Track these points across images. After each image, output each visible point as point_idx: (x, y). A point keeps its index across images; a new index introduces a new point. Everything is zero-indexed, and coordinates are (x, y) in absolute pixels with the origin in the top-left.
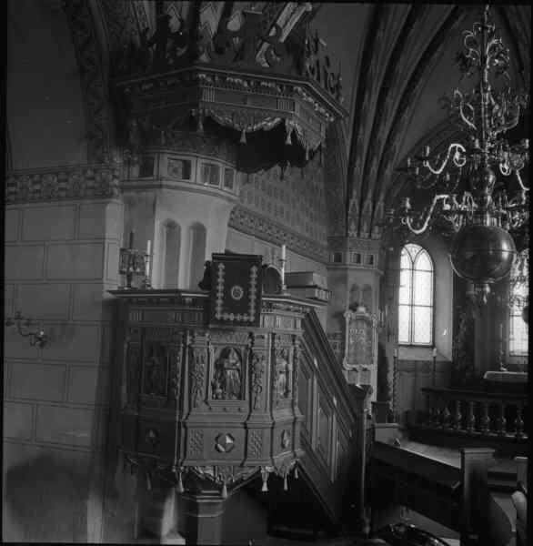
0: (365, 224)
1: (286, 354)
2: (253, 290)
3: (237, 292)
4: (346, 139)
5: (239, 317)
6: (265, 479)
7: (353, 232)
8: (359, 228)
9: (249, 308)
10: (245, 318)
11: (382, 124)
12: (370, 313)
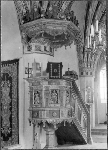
1: (68, 92)
3: (55, 70)
4: (82, 39)
5: (56, 77)
6: (65, 122)
7: (86, 66)
8: (87, 65)
9: (54, 76)
11: (89, 17)
12: (92, 89)
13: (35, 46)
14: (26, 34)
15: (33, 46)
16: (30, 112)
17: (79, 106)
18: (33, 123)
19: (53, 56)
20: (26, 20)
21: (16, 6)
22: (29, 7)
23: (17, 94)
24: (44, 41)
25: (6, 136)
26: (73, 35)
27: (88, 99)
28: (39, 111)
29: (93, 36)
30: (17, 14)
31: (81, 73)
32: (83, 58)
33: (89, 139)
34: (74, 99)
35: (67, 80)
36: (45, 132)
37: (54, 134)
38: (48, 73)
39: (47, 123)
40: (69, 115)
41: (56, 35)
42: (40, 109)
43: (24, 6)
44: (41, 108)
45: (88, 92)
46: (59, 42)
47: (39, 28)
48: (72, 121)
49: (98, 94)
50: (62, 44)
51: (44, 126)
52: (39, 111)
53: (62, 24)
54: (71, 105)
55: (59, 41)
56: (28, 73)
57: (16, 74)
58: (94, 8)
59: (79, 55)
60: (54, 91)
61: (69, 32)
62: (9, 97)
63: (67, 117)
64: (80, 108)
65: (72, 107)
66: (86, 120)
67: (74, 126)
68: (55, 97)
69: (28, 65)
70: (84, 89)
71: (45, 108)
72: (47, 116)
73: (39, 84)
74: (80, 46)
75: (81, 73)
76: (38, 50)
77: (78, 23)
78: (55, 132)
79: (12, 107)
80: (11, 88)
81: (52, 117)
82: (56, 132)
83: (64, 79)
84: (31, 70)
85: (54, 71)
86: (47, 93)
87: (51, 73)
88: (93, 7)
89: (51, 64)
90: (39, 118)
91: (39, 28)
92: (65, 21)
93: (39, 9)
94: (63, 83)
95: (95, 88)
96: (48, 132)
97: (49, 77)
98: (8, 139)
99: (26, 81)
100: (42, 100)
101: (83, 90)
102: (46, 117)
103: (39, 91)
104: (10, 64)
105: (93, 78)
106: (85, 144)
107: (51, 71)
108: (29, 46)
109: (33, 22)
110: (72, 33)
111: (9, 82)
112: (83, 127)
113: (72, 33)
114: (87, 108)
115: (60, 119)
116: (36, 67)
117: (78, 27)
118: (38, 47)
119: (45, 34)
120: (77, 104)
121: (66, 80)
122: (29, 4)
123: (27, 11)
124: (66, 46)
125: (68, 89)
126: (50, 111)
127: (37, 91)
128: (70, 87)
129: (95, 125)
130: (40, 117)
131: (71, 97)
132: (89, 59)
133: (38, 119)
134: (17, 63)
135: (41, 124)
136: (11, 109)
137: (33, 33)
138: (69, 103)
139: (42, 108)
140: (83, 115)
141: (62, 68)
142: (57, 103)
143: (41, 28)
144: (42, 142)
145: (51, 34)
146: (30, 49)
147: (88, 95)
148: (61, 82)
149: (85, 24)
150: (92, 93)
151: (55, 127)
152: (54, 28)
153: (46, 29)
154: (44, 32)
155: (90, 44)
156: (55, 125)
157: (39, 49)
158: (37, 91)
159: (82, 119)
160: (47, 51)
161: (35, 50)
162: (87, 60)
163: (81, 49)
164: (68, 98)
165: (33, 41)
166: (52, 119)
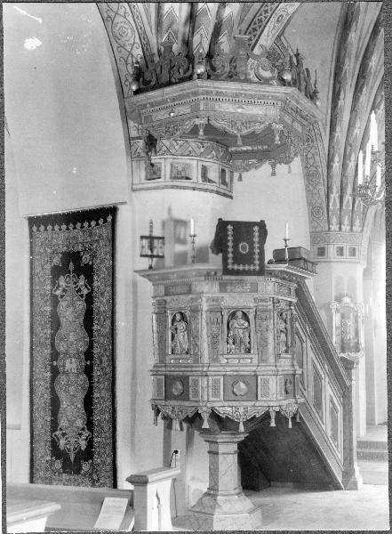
0: (346, 219)
2: (257, 245)
5: (247, 267)
6: (273, 415)
7: (334, 227)
9: (254, 259)
10: (252, 268)
11: (347, 60)
13: (172, 165)
14: (145, 125)
15: (165, 163)
16: (159, 382)
17: (316, 361)
18: (164, 418)
19: (231, 197)
20: (146, 83)
21: (110, 34)
22: (153, 40)
23: (108, 322)
24: (202, 150)
25: (72, 459)
26: (300, 129)
27: (342, 340)
28: (188, 377)
29: (376, 149)
30: (112, 62)
31: (319, 249)
32: (324, 198)
33: (348, 473)
34: (300, 337)
35: (283, 276)
36: (207, 446)
37: (235, 452)
38: (217, 254)
39: (214, 416)
40: (287, 392)
41: (245, 132)
42: (194, 369)
43: (137, 34)
44: (192, 367)
45: (343, 316)
46: (252, 151)
47: (189, 110)
48: (297, 411)
49: (375, 321)
50: (262, 156)
51: (206, 425)
52: (187, 378)
53: (264, 96)
54: (293, 358)
55: (249, 148)
56: (150, 253)
57: (108, 256)
58: (365, 32)
59: (311, 188)
60: (239, 314)
61: (288, 119)
62: (83, 333)
63: (279, 398)
64: (319, 367)
65: (295, 363)
66: (340, 408)
67: (299, 424)
68: (241, 331)
69: (151, 227)
70: (329, 304)
71: (210, 369)
72: (216, 394)
73: (189, 292)
74: (317, 157)
75: (319, 249)
76: (182, 178)
77: (315, 92)
78: (239, 447)
79: (92, 365)
80: (89, 299)
81: (232, 395)
82: (241, 445)
83: (271, 273)
84: (160, 245)
85: (238, 248)
86: (215, 320)
87: (230, 255)
88: (363, 25)
89: (230, 227)
90: (188, 399)
91: (189, 110)
92: (277, 90)
93: (187, 43)
94: (268, 287)
95: (366, 301)
96: (216, 445)
97: (221, 268)
98: (80, 468)
99: (139, 278)
100: (199, 343)
101: (327, 307)
102: (210, 398)
103: (188, 314)
104: (86, 224)
105: (359, 271)
106: (338, 488)
107: (230, 250)
108: (152, 165)
109: (168, 90)
110: (296, 125)
111: (82, 282)
112: (329, 433)
113: (296, 125)
114: (342, 371)
115: (258, 404)
116: (175, 233)
117: (317, 106)
118: (180, 169)
119: (209, 129)
120: (311, 355)
121: (277, 277)
122: (154, 28)
123: (147, 50)
124: (273, 166)
125: (283, 305)
126: (224, 376)
127: (182, 314)
128: (290, 299)
129: (367, 428)
130: (190, 396)
131: (292, 332)
132: (348, 202)
133: (187, 404)
134: (110, 218)
135: (194, 420)
136: (88, 371)
137: (171, 127)
138: (286, 352)
139: (201, 369)
140: (329, 391)
141: (265, 238)
142: (249, 352)
143: (196, 108)
144: (193, 479)
145: (229, 129)
146: (155, 173)
147: (343, 325)
148: (260, 284)
149: (334, 84)
150: (356, 318)
151: (242, 428)
152: (240, 110)
153: (212, 113)
154: (204, 121)
155: (368, 173)
156: (241, 423)
157: (183, 174)
158: (182, 314)
159: (326, 406)
160: (210, 181)
161: (171, 178)
162: (341, 206)
163: (320, 170)
164: (283, 335)
165: (164, 148)
166: (231, 403)
